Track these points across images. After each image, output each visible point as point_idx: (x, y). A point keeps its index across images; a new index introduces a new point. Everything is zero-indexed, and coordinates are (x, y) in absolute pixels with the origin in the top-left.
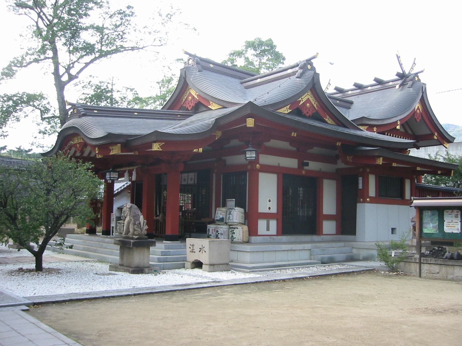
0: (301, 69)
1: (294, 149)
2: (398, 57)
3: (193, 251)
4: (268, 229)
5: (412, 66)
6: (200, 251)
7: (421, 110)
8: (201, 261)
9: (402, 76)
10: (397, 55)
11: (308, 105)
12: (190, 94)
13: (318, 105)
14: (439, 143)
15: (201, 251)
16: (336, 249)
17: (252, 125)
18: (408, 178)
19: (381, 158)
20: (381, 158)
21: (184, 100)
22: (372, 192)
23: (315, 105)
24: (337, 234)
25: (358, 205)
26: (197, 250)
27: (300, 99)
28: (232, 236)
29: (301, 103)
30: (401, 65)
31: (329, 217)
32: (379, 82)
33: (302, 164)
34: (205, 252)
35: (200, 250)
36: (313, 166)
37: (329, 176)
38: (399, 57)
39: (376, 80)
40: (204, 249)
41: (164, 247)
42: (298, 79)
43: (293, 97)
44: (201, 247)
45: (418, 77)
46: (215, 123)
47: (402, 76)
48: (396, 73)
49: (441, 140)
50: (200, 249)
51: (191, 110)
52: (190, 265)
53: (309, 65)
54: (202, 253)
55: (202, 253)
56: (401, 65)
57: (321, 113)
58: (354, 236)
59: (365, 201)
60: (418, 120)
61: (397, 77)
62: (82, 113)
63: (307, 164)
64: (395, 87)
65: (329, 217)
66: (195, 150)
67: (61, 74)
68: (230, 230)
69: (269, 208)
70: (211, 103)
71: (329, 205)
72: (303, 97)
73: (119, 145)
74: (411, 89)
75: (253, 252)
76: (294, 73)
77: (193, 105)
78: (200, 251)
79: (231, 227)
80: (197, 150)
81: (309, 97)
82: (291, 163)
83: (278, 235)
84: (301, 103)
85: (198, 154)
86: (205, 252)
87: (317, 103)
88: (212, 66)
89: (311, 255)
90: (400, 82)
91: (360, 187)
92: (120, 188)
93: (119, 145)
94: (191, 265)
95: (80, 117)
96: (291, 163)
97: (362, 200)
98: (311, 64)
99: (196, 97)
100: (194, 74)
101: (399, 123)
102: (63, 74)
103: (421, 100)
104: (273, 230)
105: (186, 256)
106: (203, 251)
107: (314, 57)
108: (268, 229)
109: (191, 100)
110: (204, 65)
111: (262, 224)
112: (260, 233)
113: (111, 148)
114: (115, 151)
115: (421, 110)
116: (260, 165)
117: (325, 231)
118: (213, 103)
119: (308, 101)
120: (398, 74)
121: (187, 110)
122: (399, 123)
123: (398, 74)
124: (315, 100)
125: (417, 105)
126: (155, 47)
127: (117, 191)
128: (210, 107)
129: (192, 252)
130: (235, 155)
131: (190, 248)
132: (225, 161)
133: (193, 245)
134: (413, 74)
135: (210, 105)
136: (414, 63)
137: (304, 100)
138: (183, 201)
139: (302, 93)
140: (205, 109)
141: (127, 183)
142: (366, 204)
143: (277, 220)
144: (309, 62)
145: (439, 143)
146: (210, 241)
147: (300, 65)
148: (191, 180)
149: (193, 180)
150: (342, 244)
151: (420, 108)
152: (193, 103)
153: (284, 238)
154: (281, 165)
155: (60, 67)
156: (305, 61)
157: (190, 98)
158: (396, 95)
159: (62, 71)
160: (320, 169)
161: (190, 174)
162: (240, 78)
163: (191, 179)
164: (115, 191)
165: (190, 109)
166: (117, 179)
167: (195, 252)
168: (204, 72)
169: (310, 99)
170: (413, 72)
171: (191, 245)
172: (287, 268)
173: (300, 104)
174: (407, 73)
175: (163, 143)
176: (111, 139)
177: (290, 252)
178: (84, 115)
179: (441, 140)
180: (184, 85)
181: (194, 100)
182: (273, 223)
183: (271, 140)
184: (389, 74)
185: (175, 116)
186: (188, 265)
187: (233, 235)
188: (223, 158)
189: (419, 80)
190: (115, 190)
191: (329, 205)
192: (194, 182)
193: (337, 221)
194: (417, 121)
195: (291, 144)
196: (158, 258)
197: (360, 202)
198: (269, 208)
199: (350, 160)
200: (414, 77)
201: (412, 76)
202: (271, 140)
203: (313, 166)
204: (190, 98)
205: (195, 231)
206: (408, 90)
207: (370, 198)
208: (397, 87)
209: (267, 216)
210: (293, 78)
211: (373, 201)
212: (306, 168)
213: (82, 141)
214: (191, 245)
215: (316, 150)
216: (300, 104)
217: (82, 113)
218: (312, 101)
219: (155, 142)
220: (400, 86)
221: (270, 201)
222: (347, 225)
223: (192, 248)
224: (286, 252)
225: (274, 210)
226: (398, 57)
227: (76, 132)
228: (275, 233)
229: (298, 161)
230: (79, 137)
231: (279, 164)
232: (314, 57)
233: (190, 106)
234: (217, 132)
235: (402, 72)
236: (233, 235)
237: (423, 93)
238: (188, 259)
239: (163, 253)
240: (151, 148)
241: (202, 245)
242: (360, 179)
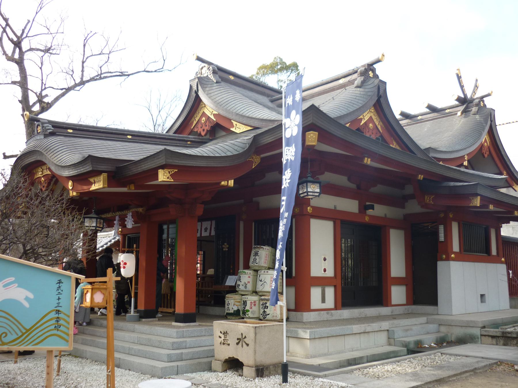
0: (361, 76)
1: (353, 186)
2: (459, 77)
3: (226, 342)
4: (323, 301)
5: (474, 90)
6: (238, 344)
7: (488, 143)
8: (241, 360)
9: (463, 101)
10: (458, 75)
11: (371, 125)
12: (204, 114)
13: (383, 126)
14: (508, 185)
15: (241, 343)
16: (416, 326)
17: (314, 142)
18: (493, 227)
19: (479, 197)
20: (479, 197)
21: (195, 123)
22: (456, 247)
23: (379, 127)
24: (407, 304)
25: (440, 264)
26: (232, 340)
27: (361, 117)
28: (264, 312)
29: (363, 122)
30: (462, 87)
31: (398, 281)
32: (432, 109)
33: (364, 208)
34: (248, 345)
35: (237, 341)
36: (379, 211)
37: (397, 224)
38: (461, 77)
39: (430, 107)
40: (245, 340)
41: (175, 335)
42: (359, 89)
43: (354, 111)
44: (240, 337)
45: (483, 101)
46: (252, 142)
47: (463, 101)
48: (456, 98)
49: (510, 181)
50: (238, 339)
51: (206, 135)
52: (221, 366)
53: (371, 72)
54: (242, 346)
55: (242, 346)
56: (462, 87)
57: (387, 136)
58: (435, 307)
59: (448, 259)
60: (486, 156)
61: (457, 103)
62: (49, 131)
63: (372, 207)
64: (457, 114)
65: (398, 281)
66: (223, 183)
67: (31, 104)
68: (261, 303)
69: (325, 270)
70: (234, 123)
71: (397, 266)
72: (364, 114)
73: (105, 175)
74: (477, 117)
75: (315, 338)
76: (351, 82)
77: (207, 128)
78: (238, 344)
79: (263, 297)
80: (226, 182)
81: (372, 114)
82: (349, 206)
83: (336, 308)
84: (363, 122)
85: (227, 187)
86: (248, 345)
87: (381, 123)
88: (232, 78)
89: (389, 338)
90: (462, 108)
91: (442, 238)
92: (106, 244)
93: (105, 175)
94: (222, 365)
95: (46, 136)
96: (349, 206)
97: (444, 256)
98: (374, 71)
99: (212, 117)
100: (209, 86)
101: (466, 158)
102: (34, 104)
103: (489, 132)
104: (330, 302)
105: (211, 348)
106: (244, 344)
107: (378, 61)
108: (323, 301)
109: (206, 122)
110: (222, 75)
111: (315, 293)
112: (313, 307)
113: (92, 180)
114: (98, 185)
115: (488, 143)
116: (312, 207)
117: (394, 301)
118: (238, 124)
119: (371, 119)
120: (459, 99)
121: (200, 135)
122: (466, 158)
123: (459, 99)
124: (379, 120)
125: (485, 138)
126: (148, 73)
127: (101, 249)
128: (233, 129)
129: (224, 344)
130: (271, 194)
131: (220, 337)
132: (258, 203)
133: (225, 333)
134: (477, 98)
135: (233, 127)
136: (476, 86)
137: (366, 118)
138: (51, 254)
139: (361, 110)
140: (224, 133)
141: (115, 238)
142: (452, 263)
143: (335, 287)
144: (372, 67)
145: (508, 185)
146: (256, 327)
147: (359, 71)
148: (206, 231)
149: (208, 231)
150: (423, 319)
151: (487, 140)
152: (208, 126)
153: (346, 313)
154: (338, 208)
155: (30, 93)
156: (366, 66)
157: (204, 119)
158: (459, 122)
159: (33, 98)
160: (385, 215)
161: (204, 223)
162: (268, 96)
163: (206, 230)
164: (99, 249)
165: (203, 134)
166: (100, 229)
167: (229, 345)
168: (223, 84)
169: (374, 117)
170: (478, 95)
171: (221, 332)
172: (374, 365)
173: (361, 124)
174: (469, 96)
175: (175, 170)
176: (93, 166)
177: (362, 335)
178: (52, 134)
179: (510, 181)
180: (194, 104)
181: (210, 122)
182: (330, 292)
183: (326, 173)
184: (447, 99)
185: (184, 143)
186: (217, 365)
187: (266, 310)
188: (255, 199)
189: (485, 105)
190: (97, 247)
191: (397, 266)
192: (210, 233)
193: (406, 285)
194: (484, 157)
195: (349, 180)
196: (168, 355)
197: (442, 260)
198: (325, 270)
199: (430, 201)
200: (479, 102)
201: (477, 100)
202: (326, 173)
203: (379, 211)
204: (204, 119)
205: (212, 302)
206: (475, 118)
207: (455, 253)
208: (459, 114)
209: (322, 282)
210: (351, 89)
211: (460, 257)
212: (370, 212)
213: (49, 173)
214: (221, 332)
215: (379, 189)
216: (361, 124)
217: (49, 131)
218: (375, 120)
219: (163, 167)
220: (462, 113)
221: (325, 259)
222: (424, 291)
223: (223, 338)
224: (358, 336)
225: (330, 273)
226: (459, 77)
227: (39, 158)
228: (332, 306)
229: (359, 203)
230: (44, 167)
231: (335, 207)
232: (378, 61)
233: (204, 130)
234: (254, 157)
235: (463, 96)
236: (266, 310)
237: (491, 121)
238: (217, 356)
239: (175, 346)
240: (157, 178)
241: (242, 334)
242: (441, 229)
